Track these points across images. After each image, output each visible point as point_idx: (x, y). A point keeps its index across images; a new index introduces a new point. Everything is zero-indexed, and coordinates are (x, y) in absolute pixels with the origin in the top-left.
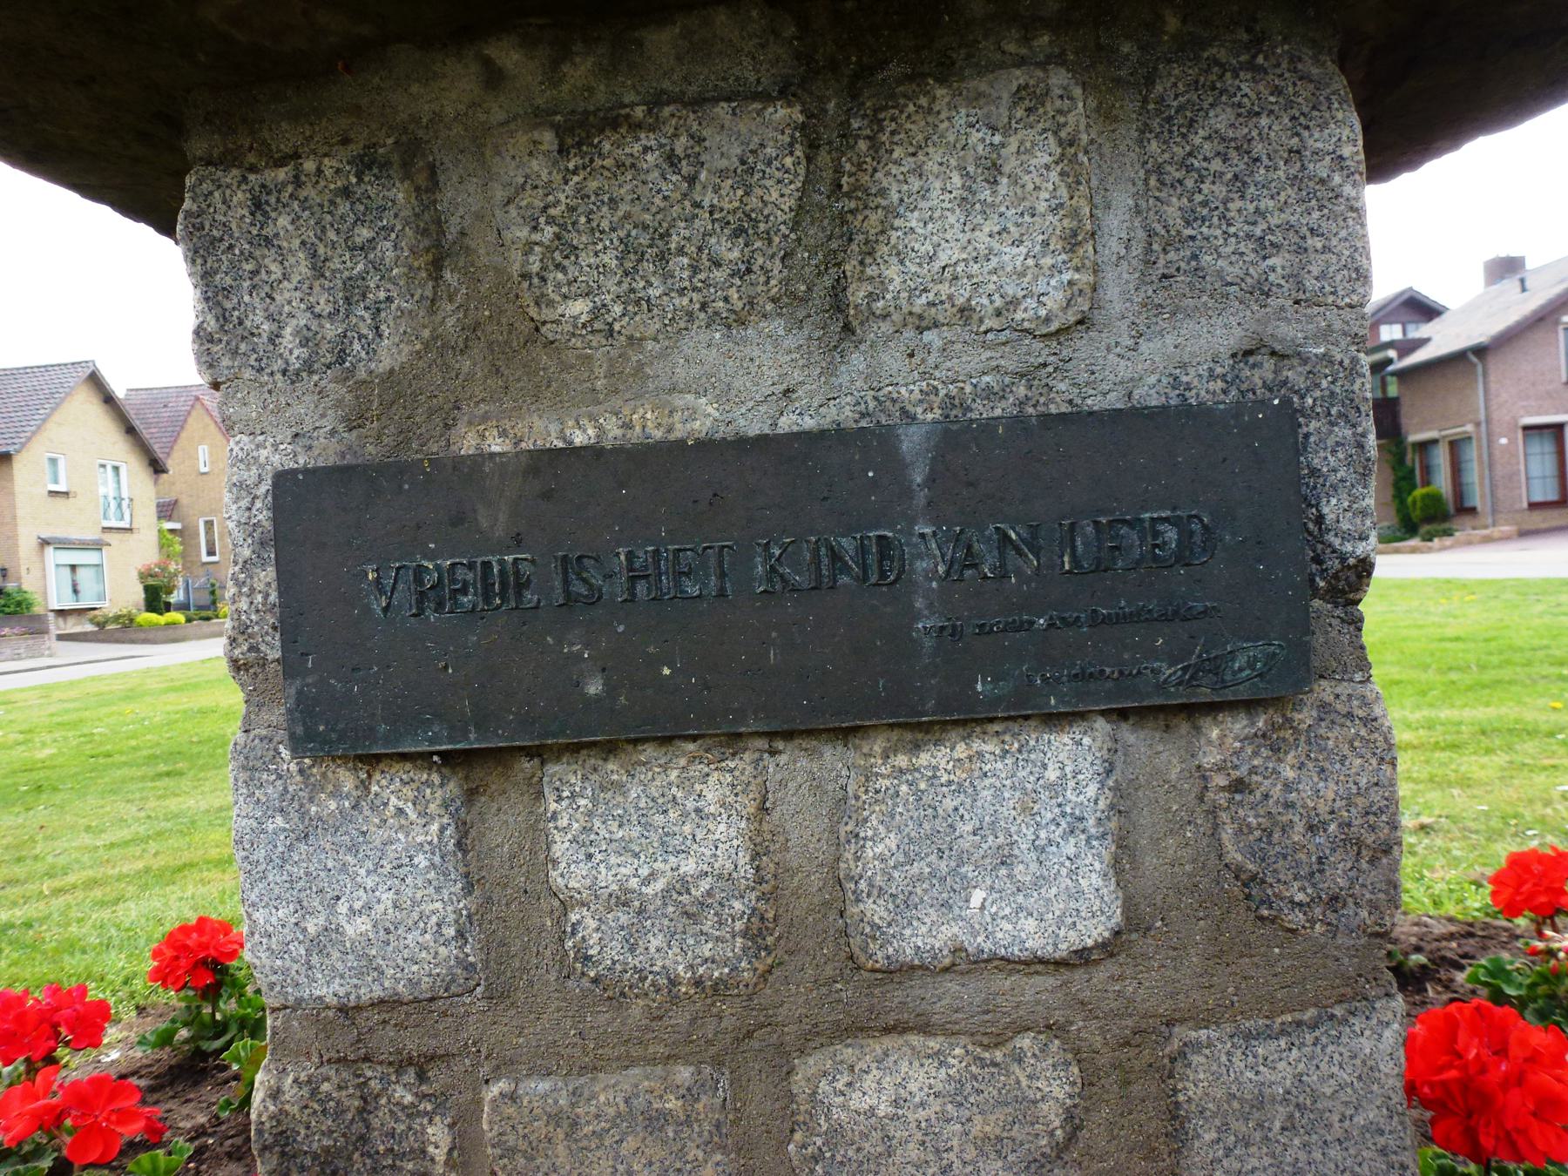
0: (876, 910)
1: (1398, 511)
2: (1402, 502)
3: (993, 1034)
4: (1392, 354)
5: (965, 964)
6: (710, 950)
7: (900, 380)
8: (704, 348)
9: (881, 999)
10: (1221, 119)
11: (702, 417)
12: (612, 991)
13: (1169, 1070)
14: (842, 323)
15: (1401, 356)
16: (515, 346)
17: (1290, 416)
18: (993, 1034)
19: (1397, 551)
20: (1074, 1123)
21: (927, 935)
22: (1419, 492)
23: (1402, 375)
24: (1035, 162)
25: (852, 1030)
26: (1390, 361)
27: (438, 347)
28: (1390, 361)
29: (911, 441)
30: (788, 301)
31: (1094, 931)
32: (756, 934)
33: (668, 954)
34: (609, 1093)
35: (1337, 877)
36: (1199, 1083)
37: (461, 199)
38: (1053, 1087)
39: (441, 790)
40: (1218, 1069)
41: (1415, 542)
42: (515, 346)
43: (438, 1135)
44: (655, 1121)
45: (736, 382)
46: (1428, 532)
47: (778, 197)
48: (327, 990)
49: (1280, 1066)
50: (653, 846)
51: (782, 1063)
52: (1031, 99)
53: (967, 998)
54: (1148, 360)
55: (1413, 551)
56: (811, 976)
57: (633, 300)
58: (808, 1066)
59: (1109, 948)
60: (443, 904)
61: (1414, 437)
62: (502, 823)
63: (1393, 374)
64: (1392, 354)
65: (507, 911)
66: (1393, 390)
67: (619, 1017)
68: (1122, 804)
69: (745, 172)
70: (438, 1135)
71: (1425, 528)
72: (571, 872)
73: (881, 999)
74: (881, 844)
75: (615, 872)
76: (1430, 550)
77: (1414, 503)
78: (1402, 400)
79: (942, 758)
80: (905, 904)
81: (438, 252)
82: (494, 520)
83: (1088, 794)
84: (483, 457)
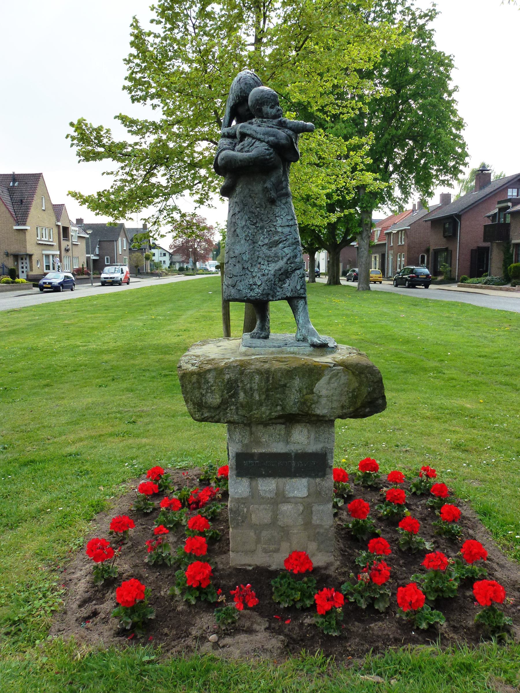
0: (287, 493)
1: (504, 272)
2: (506, 268)
3: (296, 503)
4: (510, 204)
5: (294, 497)
6: (272, 495)
7: (292, 448)
8: (275, 444)
9: (286, 500)
10: (322, 428)
11: (275, 450)
12: (263, 498)
13: (311, 507)
14: (287, 443)
15: (513, 206)
16: (258, 443)
17: (326, 453)
18: (296, 503)
19: (501, 289)
20: (303, 511)
21: (291, 495)
22: (513, 265)
23: (513, 214)
24: (305, 431)
25: (284, 502)
26: (508, 207)
27: (251, 442)
28: (508, 207)
29: (293, 454)
30: (283, 441)
31: (305, 496)
32: (276, 494)
33: (268, 495)
34: (262, 507)
35: (327, 492)
36: (314, 509)
37: (254, 429)
38: (301, 508)
39: (248, 480)
40: (315, 508)
41: (508, 286)
42: (258, 443)
43: (245, 510)
44: (266, 509)
45: (279, 448)
46: (514, 283)
47: (283, 432)
48: (237, 497)
49: (321, 507)
50: (267, 486)
51: (277, 505)
52: (305, 426)
53: (295, 501)
54: (313, 447)
55: (507, 290)
56: (280, 498)
57: (269, 440)
58: (280, 505)
59: (307, 497)
60: (248, 490)
61: (513, 242)
62: (254, 483)
63: (509, 213)
64: (510, 204)
65: (254, 493)
66: (508, 220)
67: (263, 500)
68: (309, 485)
69: (280, 430)
70: (245, 510)
71: (513, 281)
72: (260, 488)
73: (286, 500)
74: (288, 487)
75: (264, 488)
76: (514, 291)
77: (511, 269)
78: (511, 225)
79: (294, 480)
80: (289, 492)
81: (251, 433)
82: (256, 458)
83: (306, 484)
84: (255, 453)
